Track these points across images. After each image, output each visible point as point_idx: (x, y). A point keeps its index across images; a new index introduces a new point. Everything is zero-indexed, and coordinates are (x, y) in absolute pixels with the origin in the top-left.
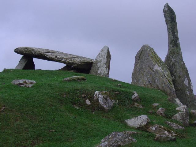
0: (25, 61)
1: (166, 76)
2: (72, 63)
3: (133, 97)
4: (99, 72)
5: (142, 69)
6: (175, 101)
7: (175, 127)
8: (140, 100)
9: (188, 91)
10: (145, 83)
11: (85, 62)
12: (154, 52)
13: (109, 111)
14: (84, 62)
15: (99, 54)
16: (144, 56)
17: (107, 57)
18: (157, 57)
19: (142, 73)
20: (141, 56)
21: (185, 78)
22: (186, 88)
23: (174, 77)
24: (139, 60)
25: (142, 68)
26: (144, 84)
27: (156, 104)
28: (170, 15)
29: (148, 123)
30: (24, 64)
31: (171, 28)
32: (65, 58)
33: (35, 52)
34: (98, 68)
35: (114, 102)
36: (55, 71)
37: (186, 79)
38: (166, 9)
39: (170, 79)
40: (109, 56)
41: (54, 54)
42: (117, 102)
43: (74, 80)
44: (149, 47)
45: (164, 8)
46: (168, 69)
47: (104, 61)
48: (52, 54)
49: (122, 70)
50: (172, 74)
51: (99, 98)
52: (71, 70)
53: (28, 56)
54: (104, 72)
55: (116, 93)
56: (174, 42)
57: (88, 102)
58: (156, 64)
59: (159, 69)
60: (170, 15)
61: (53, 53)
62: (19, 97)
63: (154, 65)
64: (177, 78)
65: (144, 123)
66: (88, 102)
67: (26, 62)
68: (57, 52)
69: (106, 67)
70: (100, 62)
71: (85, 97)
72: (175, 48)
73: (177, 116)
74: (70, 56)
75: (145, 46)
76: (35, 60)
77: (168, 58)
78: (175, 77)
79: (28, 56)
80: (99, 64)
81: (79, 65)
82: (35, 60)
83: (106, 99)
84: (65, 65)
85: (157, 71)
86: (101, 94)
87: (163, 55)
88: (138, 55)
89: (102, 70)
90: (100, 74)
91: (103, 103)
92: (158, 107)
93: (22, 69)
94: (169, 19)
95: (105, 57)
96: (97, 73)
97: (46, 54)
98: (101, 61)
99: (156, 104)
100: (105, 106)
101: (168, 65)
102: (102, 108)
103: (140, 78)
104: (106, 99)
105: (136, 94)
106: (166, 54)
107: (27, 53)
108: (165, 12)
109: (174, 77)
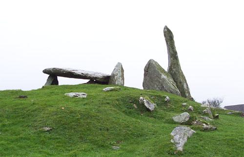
15: (115, 69)
16: (151, 69)
28: (169, 35)
29: (190, 118)
30: (51, 82)
34: (116, 80)
36: (25, 91)
38: (166, 30)
40: (122, 70)
49: (134, 80)
53: (54, 75)
56: (173, 55)
60: (169, 35)
65: (187, 119)
75: (150, 61)
76: (59, 78)
77: (170, 69)
79: (54, 75)
80: (115, 77)
82: (59, 78)
85: (164, 79)
94: (169, 38)
101: (171, 74)
102: (148, 110)
105: (168, 97)
108: (165, 32)
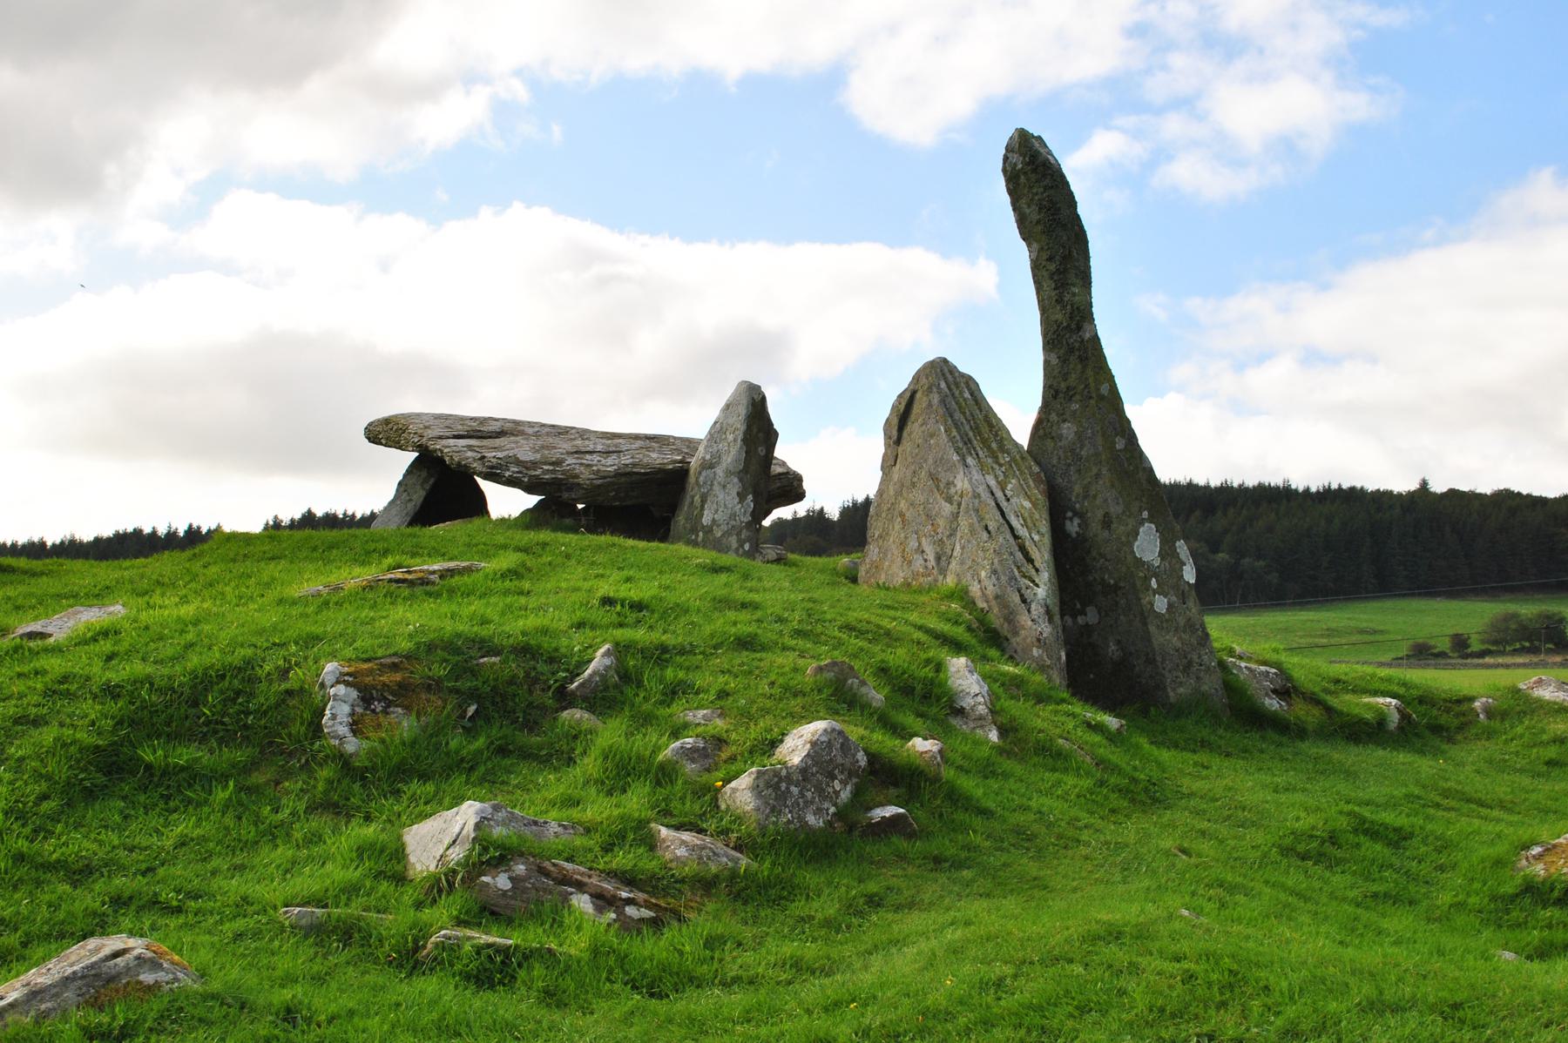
0: (425, 481)
4: (706, 519)
6: (457, 801)
9: (1161, 591)
20: (130, 569)
21: (1142, 523)
22: (1147, 579)
30: (419, 496)
54: (733, 516)
67: (428, 487)
68: (530, 431)
84: (532, 500)
87: (1017, 402)
88: (895, 421)
98: (718, 463)
106: (1036, 401)
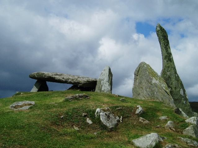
1: (164, 88)
2: (79, 83)
3: (137, 112)
4: (103, 89)
5: (141, 84)
7: (189, 143)
8: (143, 114)
10: (145, 96)
11: (90, 81)
12: (151, 68)
13: (111, 130)
14: (89, 81)
17: (109, 76)
18: (154, 72)
19: (141, 87)
23: (170, 88)
24: (137, 76)
25: (140, 83)
26: (144, 97)
27: (163, 118)
31: (164, 45)
32: (71, 79)
33: (45, 76)
34: (102, 86)
35: (118, 118)
37: (181, 89)
38: (158, 29)
39: (167, 91)
41: (62, 76)
42: (121, 119)
43: (75, 98)
44: (146, 63)
45: (156, 28)
46: (165, 82)
47: (106, 78)
48: (60, 76)
50: (169, 87)
51: (101, 116)
52: (78, 89)
55: (119, 108)
57: (89, 121)
58: (153, 78)
59: (157, 83)
61: (61, 75)
62: (6, 122)
63: (152, 79)
64: (173, 89)
66: (89, 121)
69: (108, 84)
70: (103, 80)
71: (85, 116)
72: (169, 62)
73: (188, 130)
74: (76, 77)
76: (48, 83)
77: (164, 72)
78: (172, 89)
81: (84, 84)
82: (48, 83)
83: (108, 117)
85: (156, 85)
86: (103, 111)
89: (105, 87)
90: (104, 91)
91: (105, 122)
92: (166, 121)
93: (37, 91)
94: (162, 37)
95: (107, 76)
96: (100, 90)
97: (54, 76)
99: (163, 118)
100: (108, 125)
101: (164, 78)
102: (104, 127)
103: (140, 92)
104: (108, 117)
107: (39, 77)
109: (170, 88)
